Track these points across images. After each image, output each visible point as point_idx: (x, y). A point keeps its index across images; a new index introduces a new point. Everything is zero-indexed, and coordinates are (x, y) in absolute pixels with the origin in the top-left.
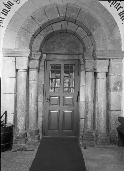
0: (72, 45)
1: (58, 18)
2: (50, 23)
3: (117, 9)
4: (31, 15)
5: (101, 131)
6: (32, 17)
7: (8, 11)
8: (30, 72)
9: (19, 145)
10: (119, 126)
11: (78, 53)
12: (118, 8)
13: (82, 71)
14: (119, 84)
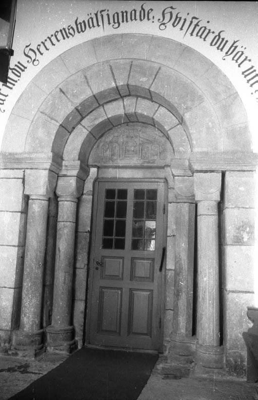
0: (150, 147)
1: (113, 89)
2: (99, 101)
3: (237, 64)
4: (60, 86)
5: (204, 340)
6: (60, 89)
7: (16, 82)
8: (60, 203)
9: (21, 358)
10: (250, 329)
11: (163, 165)
12: (239, 61)
13: (171, 203)
14: (248, 229)
